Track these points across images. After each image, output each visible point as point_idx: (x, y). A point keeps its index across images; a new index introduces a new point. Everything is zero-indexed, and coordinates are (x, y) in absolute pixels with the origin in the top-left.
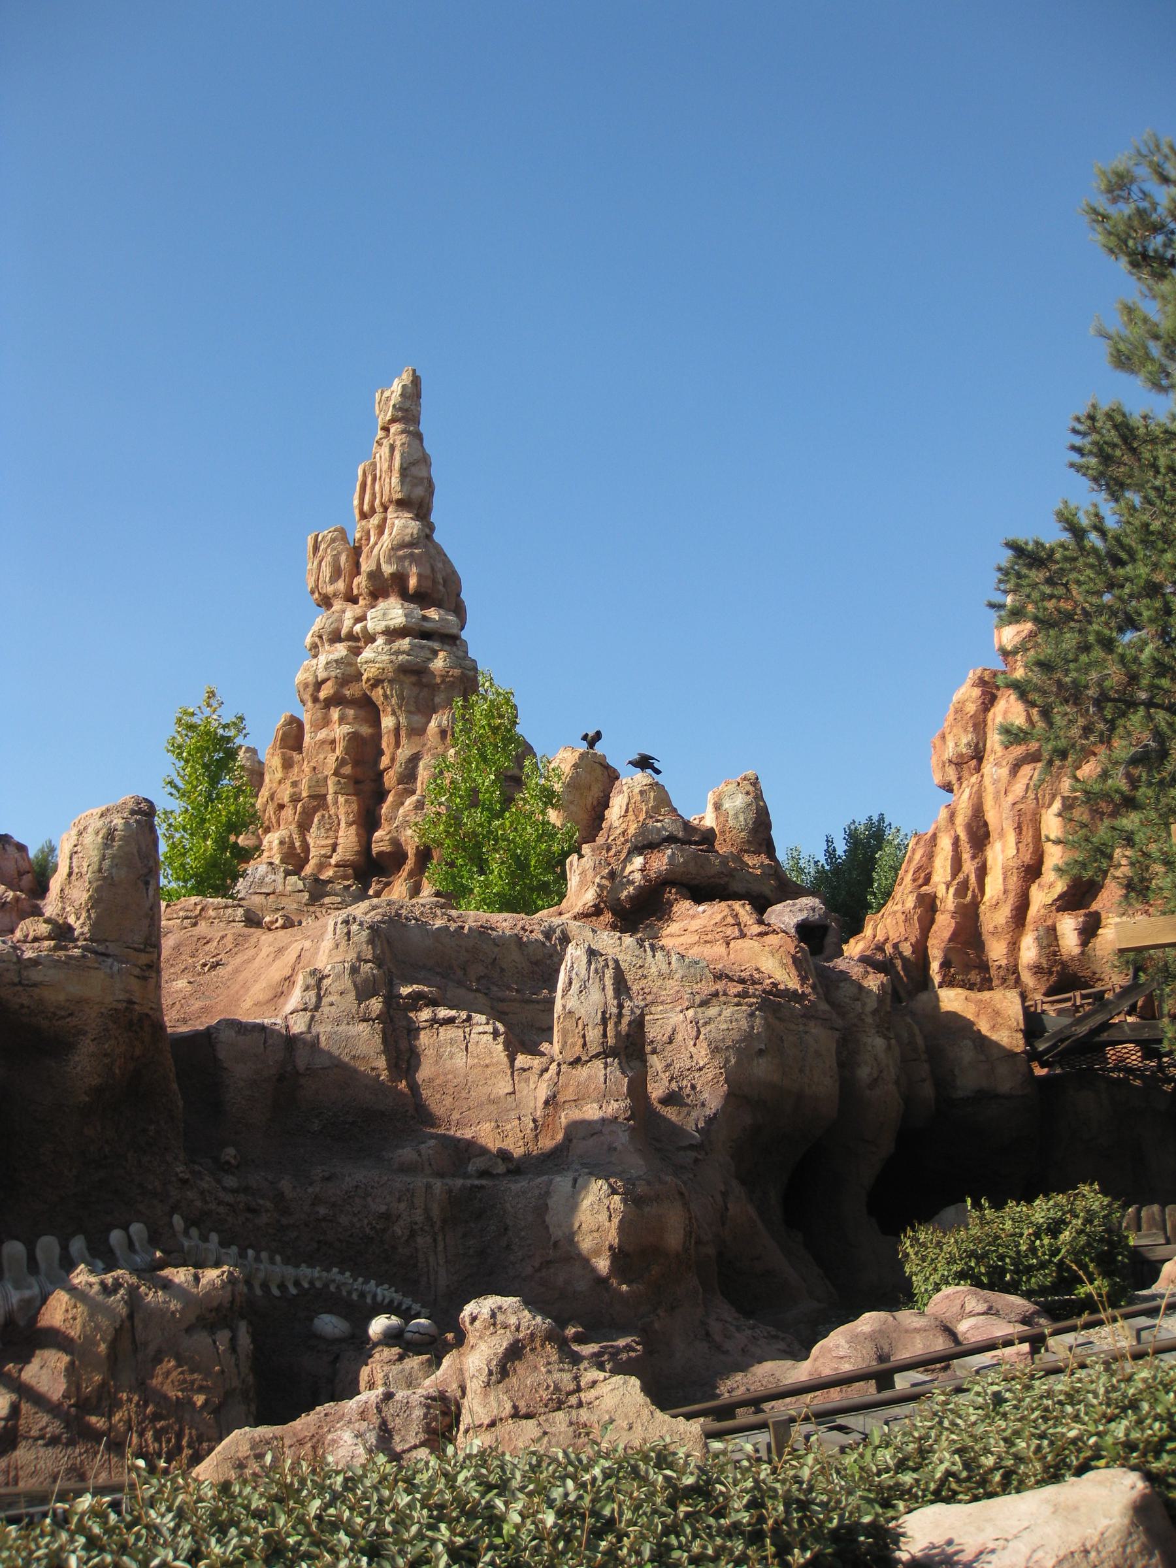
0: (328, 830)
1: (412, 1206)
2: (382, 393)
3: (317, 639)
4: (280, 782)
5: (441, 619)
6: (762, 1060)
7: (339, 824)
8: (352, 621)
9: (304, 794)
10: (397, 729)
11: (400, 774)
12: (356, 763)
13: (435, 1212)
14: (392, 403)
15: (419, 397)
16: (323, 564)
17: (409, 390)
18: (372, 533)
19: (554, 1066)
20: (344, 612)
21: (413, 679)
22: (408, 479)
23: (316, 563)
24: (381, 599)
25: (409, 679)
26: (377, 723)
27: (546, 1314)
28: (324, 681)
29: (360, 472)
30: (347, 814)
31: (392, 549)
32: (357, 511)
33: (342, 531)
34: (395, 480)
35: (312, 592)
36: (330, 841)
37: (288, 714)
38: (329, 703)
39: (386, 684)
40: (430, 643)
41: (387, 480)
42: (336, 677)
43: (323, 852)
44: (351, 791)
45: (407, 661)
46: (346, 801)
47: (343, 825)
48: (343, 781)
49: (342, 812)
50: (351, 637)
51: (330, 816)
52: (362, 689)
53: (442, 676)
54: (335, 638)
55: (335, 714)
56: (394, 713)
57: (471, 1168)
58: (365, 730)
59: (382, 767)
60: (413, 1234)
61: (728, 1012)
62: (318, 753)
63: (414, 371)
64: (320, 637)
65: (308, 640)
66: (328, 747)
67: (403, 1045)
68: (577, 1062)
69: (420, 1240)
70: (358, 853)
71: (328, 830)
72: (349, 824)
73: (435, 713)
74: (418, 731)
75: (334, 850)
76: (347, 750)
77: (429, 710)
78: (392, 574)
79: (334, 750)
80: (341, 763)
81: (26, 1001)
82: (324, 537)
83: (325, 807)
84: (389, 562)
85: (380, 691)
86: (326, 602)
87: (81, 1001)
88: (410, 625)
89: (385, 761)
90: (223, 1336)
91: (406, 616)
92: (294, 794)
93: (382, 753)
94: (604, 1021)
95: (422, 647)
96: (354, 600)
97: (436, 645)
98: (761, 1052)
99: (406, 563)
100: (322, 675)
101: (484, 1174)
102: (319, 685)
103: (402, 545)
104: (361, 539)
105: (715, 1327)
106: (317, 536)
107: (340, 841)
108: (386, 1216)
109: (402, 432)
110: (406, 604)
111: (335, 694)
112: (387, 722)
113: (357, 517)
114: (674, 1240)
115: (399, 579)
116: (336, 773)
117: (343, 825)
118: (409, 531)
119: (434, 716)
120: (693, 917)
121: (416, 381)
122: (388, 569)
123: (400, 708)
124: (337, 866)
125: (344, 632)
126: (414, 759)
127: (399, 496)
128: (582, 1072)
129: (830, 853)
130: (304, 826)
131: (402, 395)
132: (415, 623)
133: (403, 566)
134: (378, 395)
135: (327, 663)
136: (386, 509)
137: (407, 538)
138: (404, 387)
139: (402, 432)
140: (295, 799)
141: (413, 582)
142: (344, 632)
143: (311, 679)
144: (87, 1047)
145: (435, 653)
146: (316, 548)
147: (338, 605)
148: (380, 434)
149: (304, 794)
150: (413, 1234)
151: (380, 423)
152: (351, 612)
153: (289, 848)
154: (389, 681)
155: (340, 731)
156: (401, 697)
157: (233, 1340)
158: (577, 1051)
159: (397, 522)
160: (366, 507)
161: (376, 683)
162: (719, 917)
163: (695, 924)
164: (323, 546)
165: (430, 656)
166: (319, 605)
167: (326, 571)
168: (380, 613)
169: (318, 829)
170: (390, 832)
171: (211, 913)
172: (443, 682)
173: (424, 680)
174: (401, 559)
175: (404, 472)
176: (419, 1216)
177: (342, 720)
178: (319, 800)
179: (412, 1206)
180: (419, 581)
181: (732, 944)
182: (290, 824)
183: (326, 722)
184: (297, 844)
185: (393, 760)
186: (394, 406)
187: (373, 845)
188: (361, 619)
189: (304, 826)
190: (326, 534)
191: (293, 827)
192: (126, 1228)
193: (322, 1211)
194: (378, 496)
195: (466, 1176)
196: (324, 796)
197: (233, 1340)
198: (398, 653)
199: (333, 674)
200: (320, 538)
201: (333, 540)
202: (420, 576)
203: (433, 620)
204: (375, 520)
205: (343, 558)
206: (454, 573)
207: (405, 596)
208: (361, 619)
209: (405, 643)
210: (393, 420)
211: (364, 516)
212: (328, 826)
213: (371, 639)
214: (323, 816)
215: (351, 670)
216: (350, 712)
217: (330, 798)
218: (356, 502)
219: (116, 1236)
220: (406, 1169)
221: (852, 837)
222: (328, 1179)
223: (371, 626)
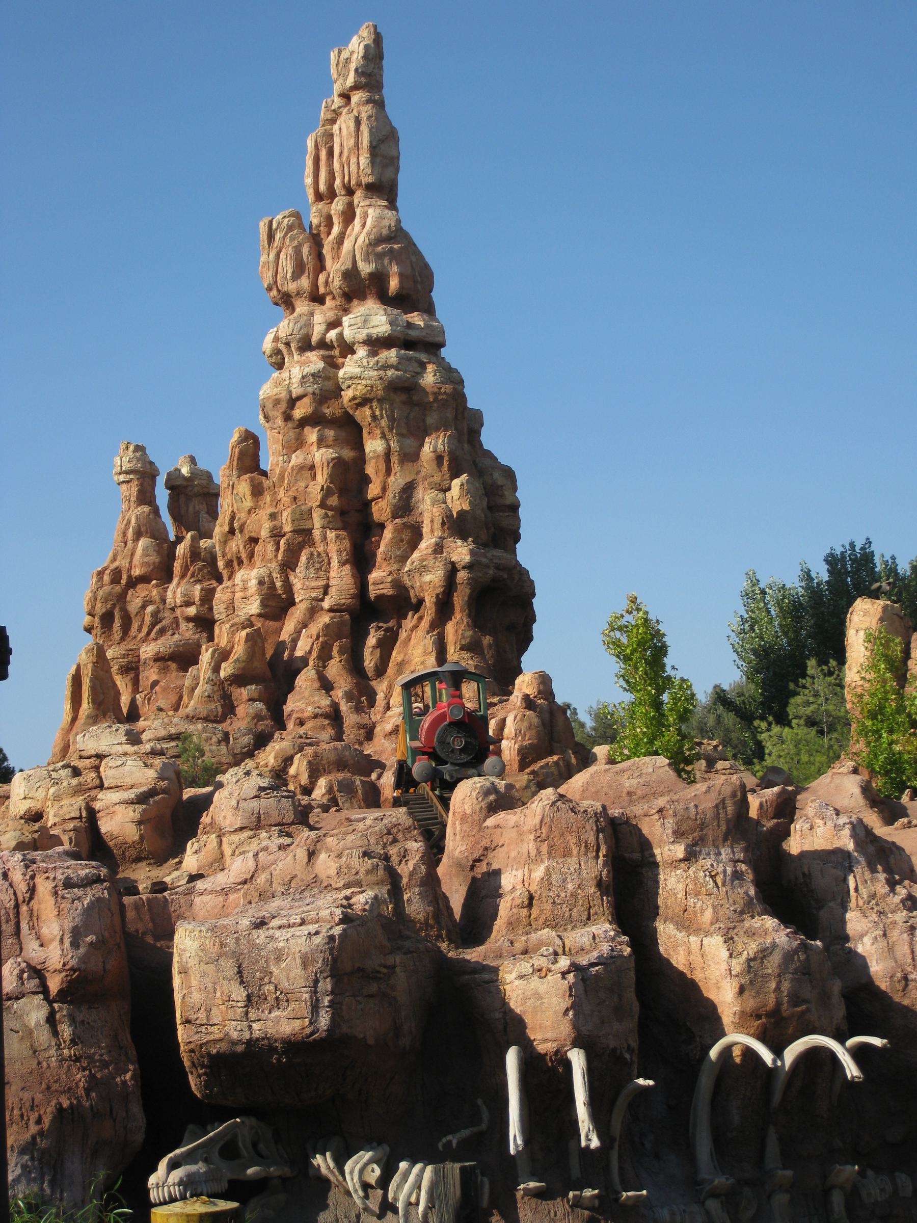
0: (318, 570)
2: (340, 52)
3: (281, 346)
4: (250, 512)
5: (427, 326)
7: (329, 563)
8: (324, 327)
9: (287, 528)
10: (388, 454)
11: (395, 506)
12: (343, 491)
14: (353, 66)
15: (381, 57)
16: (282, 256)
17: (372, 51)
18: (336, 220)
20: (312, 314)
21: (403, 397)
22: (378, 160)
23: (272, 256)
24: (355, 302)
25: (399, 398)
26: (359, 446)
27: (742, 1061)
28: (299, 398)
29: (310, 144)
30: (339, 551)
31: (370, 244)
32: (310, 192)
33: (297, 215)
34: (364, 160)
35: (269, 289)
36: (322, 583)
37: (243, 429)
38: (304, 422)
39: (375, 404)
40: (417, 355)
41: (353, 160)
42: (314, 394)
43: (313, 595)
44: (340, 525)
45: (397, 376)
46: (337, 537)
47: (335, 563)
48: (330, 513)
49: (333, 549)
50: (323, 344)
51: (319, 554)
52: (343, 407)
53: (434, 394)
54: (306, 345)
55: (312, 435)
56: (383, 436)
58: (348, 454)
59: (370, 496)
62: (297, 481)
63: (375, 27)
64: (288, 344)
65: (268, 344)
66: (307, 474)
70: (354, 596)
71: (318, 570)
72: (342, 564)
73: (429, 435)
74: (411, 457)
75: (326, 593)
76: (332, 477)
77: (421, 433)
78: (371, 275)
79: (314, 477)
80: (327, 493)
82: (279, 224)
83: (310, 542)
84: (367, 259)
85: (368, 412)
86: (286, 301)
88: (396, 334)
89: (373, 490)
91: (391, 323)
92: (275, 528)
93: (367, 480)
95: (409, 359)
96: (318, 299)
97: (423, 357)
99: (386, 261)
100: (296, 391)
102: (292, 402)
103: (380, 240)
104: (319, 226)
106: (271, 222)
109: (368, 102)
110: (389, 309)
111: (314, 413)
112: (374, 446)
113: (311, 197)
115: (378, 281)
116: (322, 505)
117: (335, 563)
118: (386, 222)
119: (427, 440)
121: (378, 39)
122: (366, 268)
123: (391, 430)
124: (331, 610)
125: (315, 339)
126: (408, 489)
127: (370, 179)
129: (807, 576)
130: (288, 565)
131: (365, 57)
132: (401, 332)
133: (383, 264)
134: (333, 55)
135: (303, 377)
136: (350, 192)
137: (385, 232)
138: (367, 47)
139: (368, 102)
140: (276, 534)
141: (394, 284)
142: (315, 339)
143: (284, 395)
145: (423, 366)
146: (271, 237)
147: (302, 307)
148: (338, 102)
149: (287, 528)
151: (337, 88)
152: (320, 317)
153: (269, 588)
154: (378, 400)
155: (321, 456)
156: (392, 419)
159: (371, 211)
160: (322, 187)
161: (364, 401)
164: (278, 236)
165: (419, 370)
166: (276, 304)
167: (287, 265)
168: (360, 320)
169: (307, 568)
170: (390, 574)
172: (436, 399)
173: (415, 398)
174: (380, 257)
175: (374, 149)
177: (321, 442)
178: (304, 535)
180: (401, 282)
182: (270, 561)
183: (299, 443)
184: (278, 584)
185: (384, 489)
186: (356, 70)
187: (371, 588)
188: (335, 324)
189: (288, 565)
190: (281, 218)
191: (274, 565)
194: (338, 175)
196: (309, 532)
198: (385, 367)
199: (310, 390)
200: (274, 226)
201: (290, 228)
202: (401, 276)
203: (417, 327)
204: (338, 205)
205: (305, 250)
206: (426, 266)
207: (384, 298)
208: (335, 324)
209: (391, 355)
210: (355, 87)
211: (319, 197)
212: (317, 566)
213: (348, 349)
214: (312, 554)
215: (329, 385)
216: (330, 433)
217: (317, 533)
218: (309, 181)
223: (348, 334)
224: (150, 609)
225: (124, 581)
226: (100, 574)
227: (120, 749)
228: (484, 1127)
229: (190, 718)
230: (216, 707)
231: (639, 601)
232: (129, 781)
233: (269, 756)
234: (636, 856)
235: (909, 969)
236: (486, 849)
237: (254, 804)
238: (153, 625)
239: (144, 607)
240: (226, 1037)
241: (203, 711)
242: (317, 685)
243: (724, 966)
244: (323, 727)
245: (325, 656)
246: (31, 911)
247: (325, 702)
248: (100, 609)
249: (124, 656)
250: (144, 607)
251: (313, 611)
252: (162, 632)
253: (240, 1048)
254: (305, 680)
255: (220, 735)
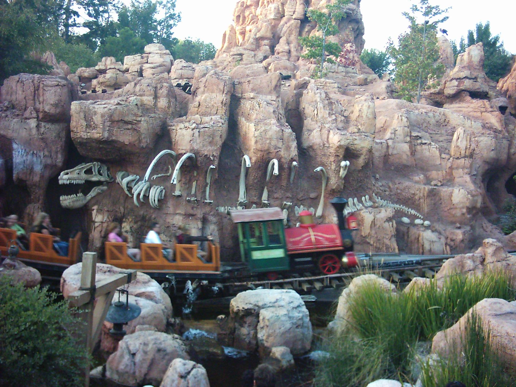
1: (420, 192)
6: (492, 152)
13: (426, 195)
19: (451, 158)
36: (293, 10)
57: (432, 183)
60: (420, 199)
61: (486, 138)
67: (413, 149)
68: (458, 158)
69: (421, 200)
81: (353, 148)
87: (363, 147)
90: (391, 223)
94: (466, 148)
98: (493, 150)
101: (435, 185)
105: (484, 225)
107: (296, 10)
108: (414, 194)
114: (479, 205)
117: (298, 4)
120: (472, 103)
128: (459, 161)
144: (362, 157)
150: (420, 199)
157: (392, 224)
158: (458, 155)
162: (479, 105)
163: (472, 105)
171: (328, 85)
176: (421, 195)
179: (420, 192)
181: (483, 113)
184: (281, 9)
192: (365, 196)
193: (399, 191)
195: (431, 185)
197: (392, 224)
219: (363, 198)
220: (417, 182)
221: (479, 28)
222: (399, 183)
224: (251, 15)
225: (245, 6)
226: (238, 3)
227: (156, 52)
228: (169, 174)
229: (245, 49)
230: (254, 47)
231: (493, 34)
232: (155, 61)
233: (264, 63)
234: (240, 95)
235: (325, 143)
236: (197, 88)
237: (180, 71)
238: (251, 20)
239: (249, 15)
240: (81, 137)
241: (249, 48)
242: (285, 42)
243: (253, 133)
244: (284, 56)
245: (290, 34)
246: (38, 93)
247: (287, 48)
248: (236, 14)
249: (241, 29)
250: (249, 15)
251: (289, 20)
252: (253, 23)
253: (85, 141)
254: (282, 41)
255: (253, 55)
